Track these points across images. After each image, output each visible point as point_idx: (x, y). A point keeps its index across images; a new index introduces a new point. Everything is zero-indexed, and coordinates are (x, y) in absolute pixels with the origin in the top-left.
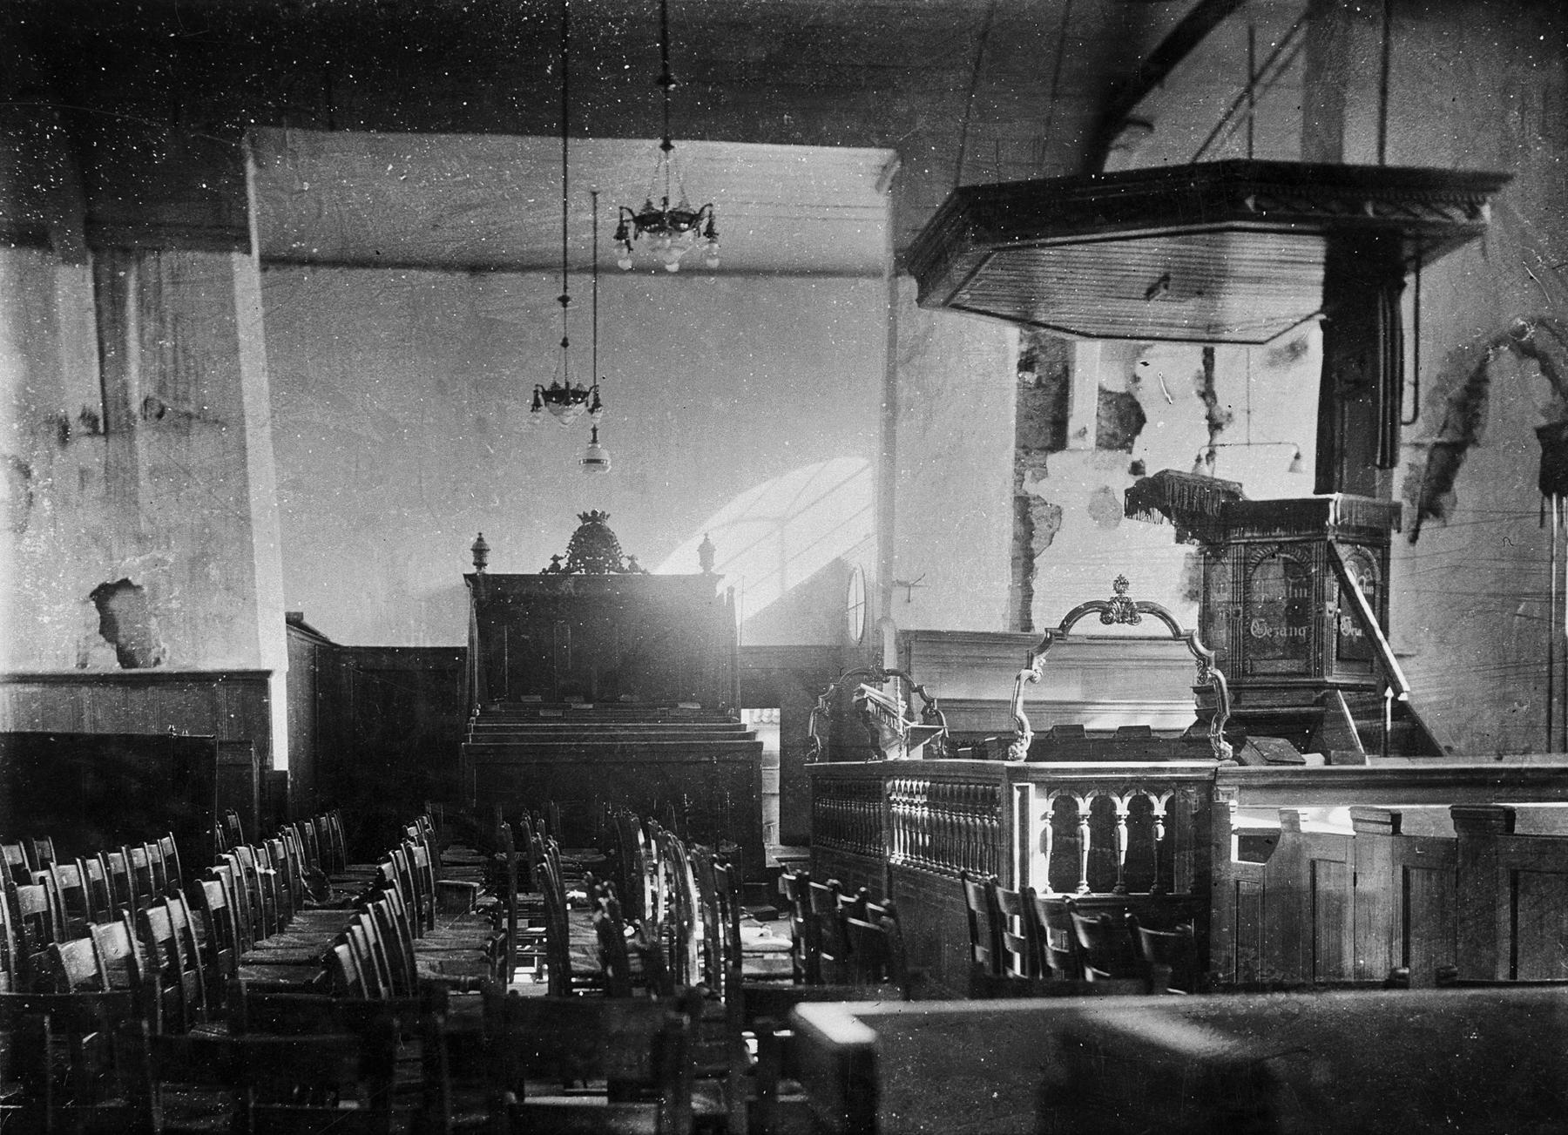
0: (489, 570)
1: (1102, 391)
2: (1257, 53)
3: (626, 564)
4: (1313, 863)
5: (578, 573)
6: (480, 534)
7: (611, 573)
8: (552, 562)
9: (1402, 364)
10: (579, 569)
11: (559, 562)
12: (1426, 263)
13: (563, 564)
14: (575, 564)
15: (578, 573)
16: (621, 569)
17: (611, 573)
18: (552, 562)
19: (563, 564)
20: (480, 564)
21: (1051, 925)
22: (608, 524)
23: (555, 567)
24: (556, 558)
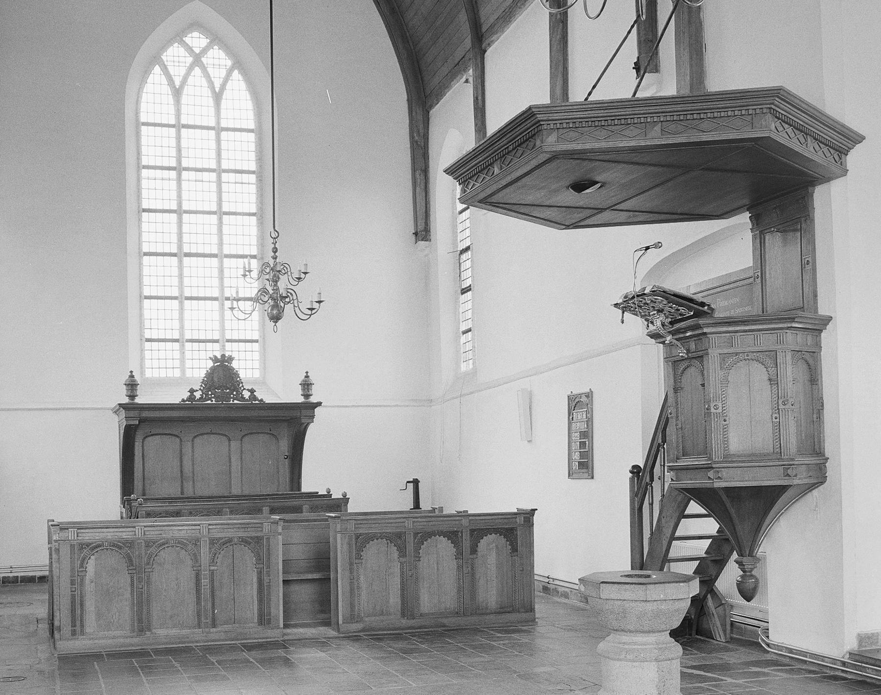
0: (138, 400)
1: (534, 511)
2: (500, 194)
3: (246, 395)
4: (701, 339)
5: (209, 402)
6: (131, 372)
7: (236, 402)
8: (189, 394)
9: (755, 324)
10: (210, 399)
11: (195, 393)
12: (431, 107)
13: (198, 395)
14: (207, 395)
15: (209, 402)
16: (243, 398)
17: (236, 402)
18: (189, 394)
19: (198, 395)
20: (132, 397)
21: (767, 677)
22: (235, 365)
23: (191, 398)
24: (192, 391)
